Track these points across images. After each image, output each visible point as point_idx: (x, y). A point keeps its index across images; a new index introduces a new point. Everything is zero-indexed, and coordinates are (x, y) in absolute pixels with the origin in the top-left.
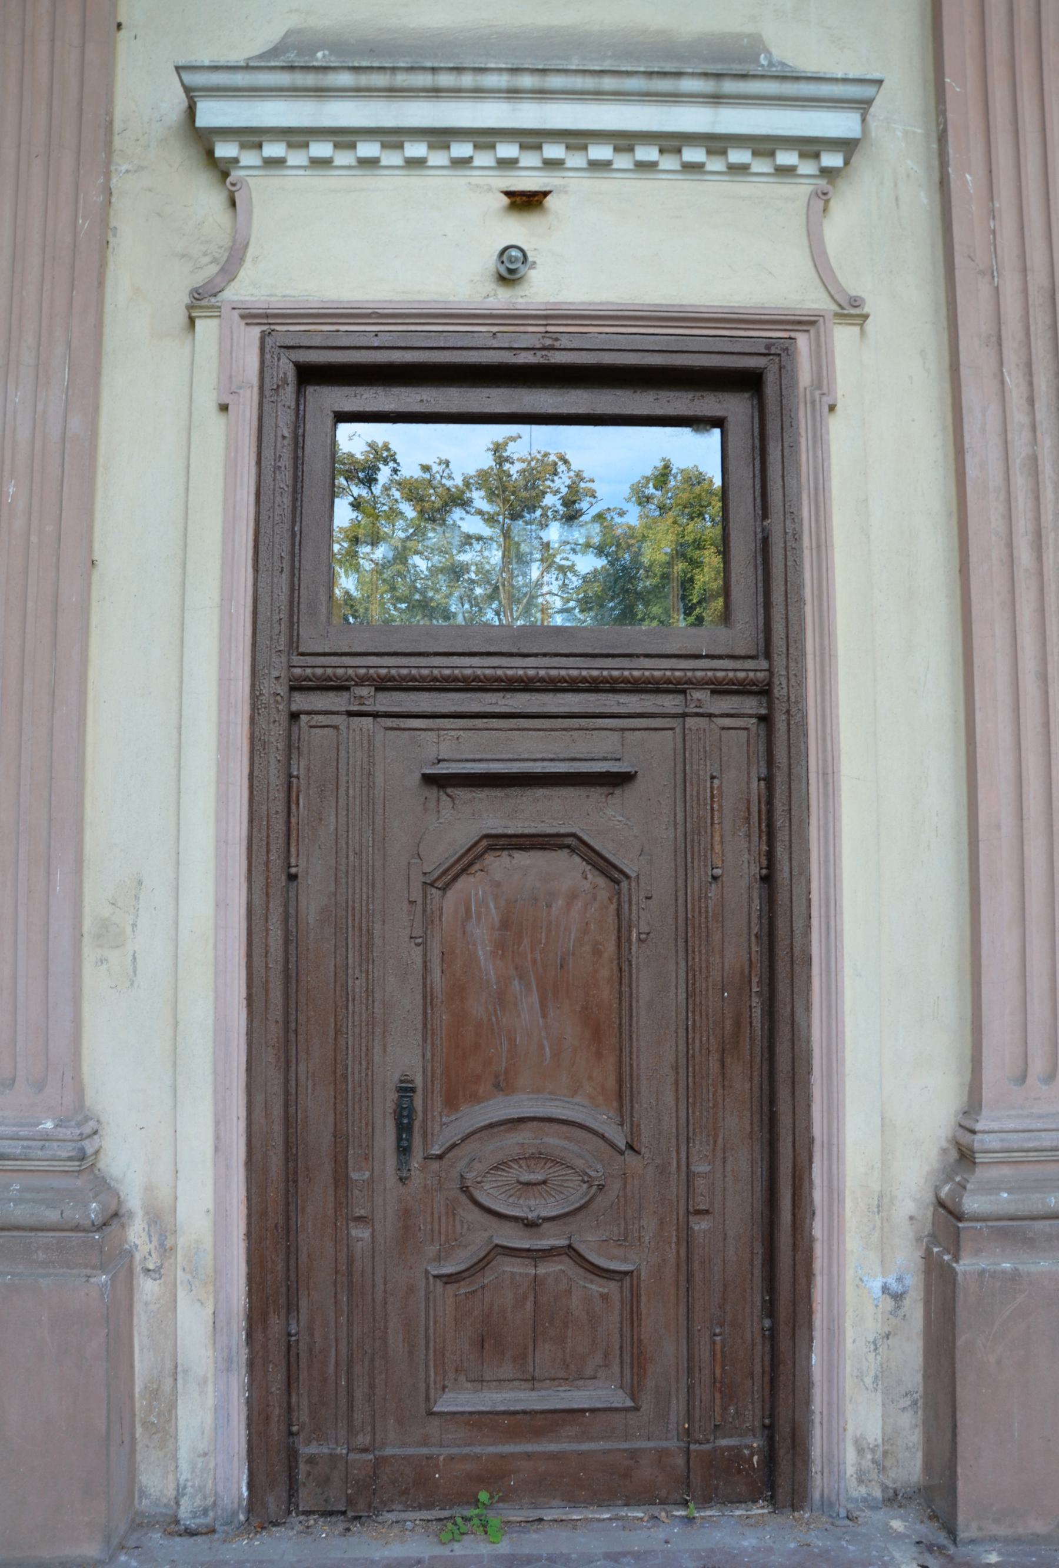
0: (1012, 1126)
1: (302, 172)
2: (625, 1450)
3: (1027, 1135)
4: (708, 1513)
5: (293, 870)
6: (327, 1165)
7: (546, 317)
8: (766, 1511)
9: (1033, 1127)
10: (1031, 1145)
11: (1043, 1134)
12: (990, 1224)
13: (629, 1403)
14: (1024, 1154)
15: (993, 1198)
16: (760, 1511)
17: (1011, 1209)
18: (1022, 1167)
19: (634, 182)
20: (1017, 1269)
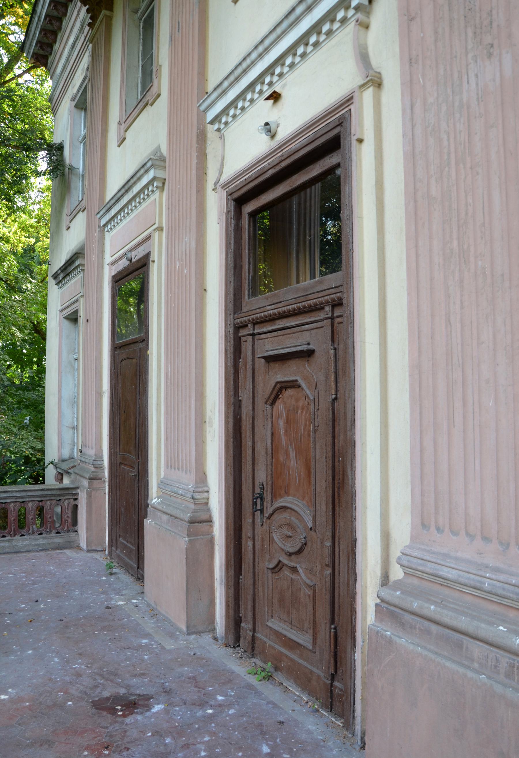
0: (415, 554)
1: (250, 107)
2: (309, 669)
3: (420, 561)
4: (324, 713)
5: (240, 398)
6: (31, 518)
7: (280, 147)
8: (341, 725)
9: (425, 558)
10: (420, 568)
11: (429, 564)
12: (390, 607)
13: (311, 648)
14: (421, 573)
15: (392, 592)
16: (340, 724)
17: (396, 601)
18: (424, 582)
19: (291, 75)
20: (391, 638)
